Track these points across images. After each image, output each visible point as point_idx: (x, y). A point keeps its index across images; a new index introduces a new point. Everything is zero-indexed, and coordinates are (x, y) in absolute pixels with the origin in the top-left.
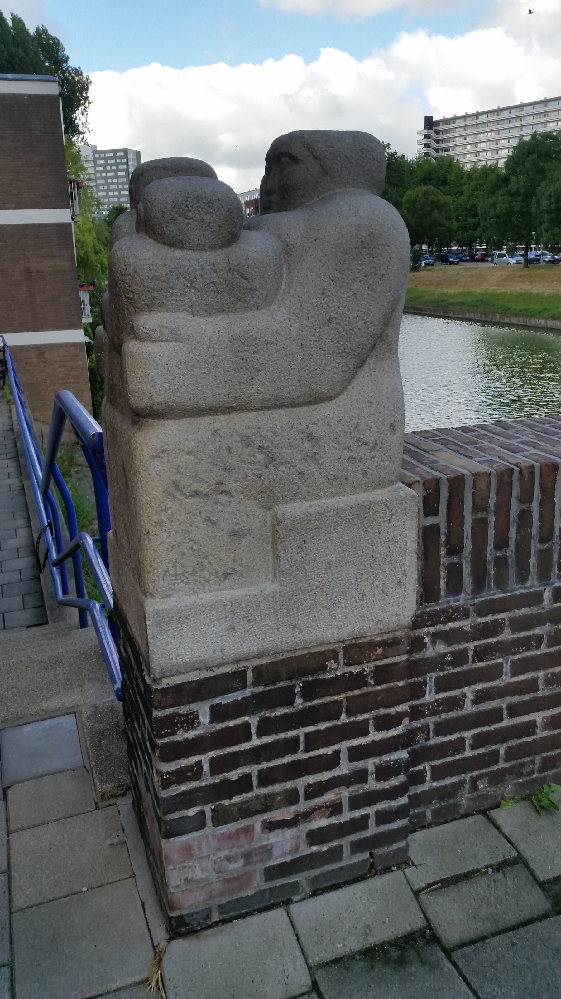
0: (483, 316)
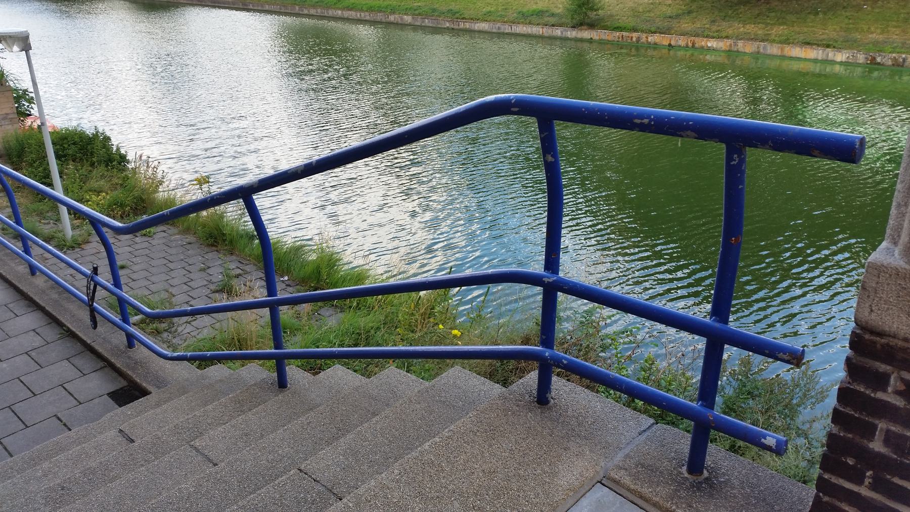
0: (283, 8)
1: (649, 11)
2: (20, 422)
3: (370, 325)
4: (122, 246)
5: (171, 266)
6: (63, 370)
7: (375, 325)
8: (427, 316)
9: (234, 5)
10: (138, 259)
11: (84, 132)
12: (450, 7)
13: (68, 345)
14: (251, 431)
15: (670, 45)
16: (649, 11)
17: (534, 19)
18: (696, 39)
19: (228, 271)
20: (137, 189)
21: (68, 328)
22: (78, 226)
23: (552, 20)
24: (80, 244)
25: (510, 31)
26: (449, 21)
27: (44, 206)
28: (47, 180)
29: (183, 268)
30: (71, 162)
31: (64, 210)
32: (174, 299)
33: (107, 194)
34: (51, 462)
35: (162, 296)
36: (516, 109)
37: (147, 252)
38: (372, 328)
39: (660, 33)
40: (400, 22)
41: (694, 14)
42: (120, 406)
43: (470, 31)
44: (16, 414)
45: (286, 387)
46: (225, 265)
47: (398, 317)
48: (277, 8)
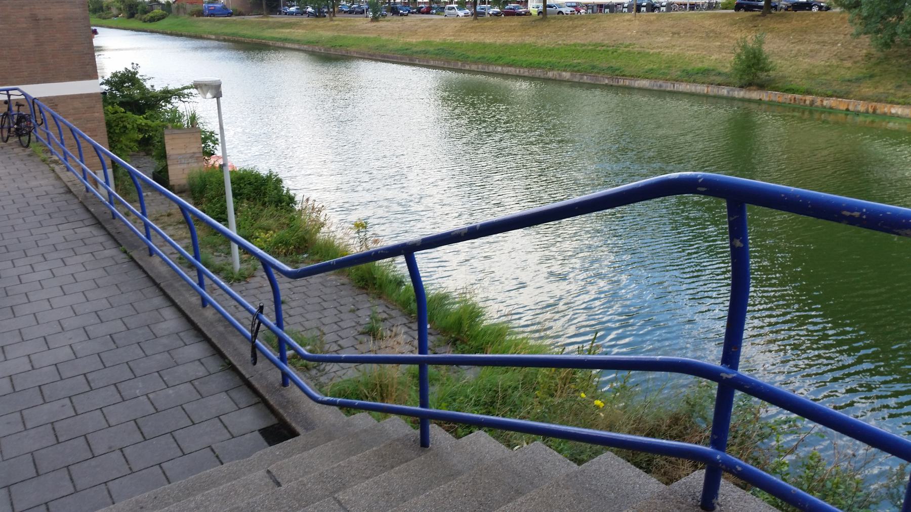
0: (446, 64)
1: (825, 74)
2: (179, 450)
3: (509, 383)
4: (284, 284)
5: (325, 305)
6: (220, 402)
7: (513, 384)
8: (568, 381)
9: (401, 59)
10: (296, 295)
11: (259, 174)
12: (611, 65)
13: (229, 377)
14: (393, 490)
15: (847, 110)
16: (825, 74)
17: (699, 77)
18: (878, 105)
19: (376, 315)
20: (301, 229)
21: (230, 361)
22: (246, 261)
23: (719, 79)
24: (245, 278)
25: (672, 89)
26: (608, 78)
27: (217, 240)
28: (223, 216)
29: (335, 308)
30: (245, 201)
31: (235, 247)
32: (324, 338)
33: (274, 232)
34: (203, 496)
35: (314, 333)
36: (703, 189)
37: (305, 289)
38: (509, 387)
39: (837, 97)
40: (558, 77)
41: (877, 78)
42: (270, 444)
43: (630, 89)
44: (176, 441)
45: (428, 446)
46: (374, 308)
47: (536, 378)
48: (440, 64)
